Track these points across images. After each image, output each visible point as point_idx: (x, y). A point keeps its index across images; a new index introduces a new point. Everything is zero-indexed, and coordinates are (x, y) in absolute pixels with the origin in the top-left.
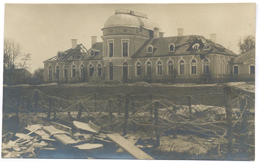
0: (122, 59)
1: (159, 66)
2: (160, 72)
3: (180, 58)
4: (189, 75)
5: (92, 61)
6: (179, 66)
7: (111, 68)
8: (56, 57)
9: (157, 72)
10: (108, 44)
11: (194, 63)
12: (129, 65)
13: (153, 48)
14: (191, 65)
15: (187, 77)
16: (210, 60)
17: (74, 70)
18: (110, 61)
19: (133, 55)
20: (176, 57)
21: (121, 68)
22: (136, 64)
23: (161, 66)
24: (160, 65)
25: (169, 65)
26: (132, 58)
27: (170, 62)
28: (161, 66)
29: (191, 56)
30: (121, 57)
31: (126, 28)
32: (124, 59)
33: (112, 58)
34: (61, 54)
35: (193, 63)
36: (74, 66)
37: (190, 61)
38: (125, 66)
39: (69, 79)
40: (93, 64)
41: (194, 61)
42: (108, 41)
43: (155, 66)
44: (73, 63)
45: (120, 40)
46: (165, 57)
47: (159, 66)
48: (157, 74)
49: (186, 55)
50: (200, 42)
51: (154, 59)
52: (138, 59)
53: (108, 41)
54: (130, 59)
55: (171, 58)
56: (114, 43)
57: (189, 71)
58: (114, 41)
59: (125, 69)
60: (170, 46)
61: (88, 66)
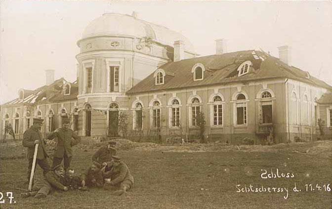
0: (108, 96)
1: (175, 109)
2: (176, 121)
3: (172, 96)
4: (232, 126)
5: (64, 103)
6: (170, 110)
7: (89, 114)
8: (301, 79)
9: (170, 120)
10: (84, 69)
11: (242, 101)
12: (121, 109)
13: (164, 75)
14: (234, 104)
15: (227, 131)
16: (275, 94)
17: (139, 113)
18: (86, 102)
19: (130, 89)
20: (229, 86)
21: (106, 113)
22: (134, 106)
23: (220, 106)
24: (176, 106)
25: (193, 106)
26: (127, 94)
27: (195, 99)
28: (220, 106)
29: (171, 92)
30: (106, 93)
31: (116, 38)
32: (110, 96)
33: (89, 94)
34: (70, 87)
35: (239, 101)
36: (139, 104)
37: (234, 98)
38: (114, 109)
39: (206, 135)
40: (143, 102)
41: (241, 97)
42: (85, 64)
43: (167, 109)
44: (38, 107)
45: (105, 61)
46: (184, 91)
47: (175, 109)
48: (170, 124)
49: (225, 84)
50: (251, 58)
51: (164, 95)
52: (138, 97)
53: (84, 65)
54: (123, 96)
55: (156, 96)
56: (93, 68)
57: (232, 119)
58: (93, 63)
59: (113, 116)
60: (195, 69)
61: (59, 113)
